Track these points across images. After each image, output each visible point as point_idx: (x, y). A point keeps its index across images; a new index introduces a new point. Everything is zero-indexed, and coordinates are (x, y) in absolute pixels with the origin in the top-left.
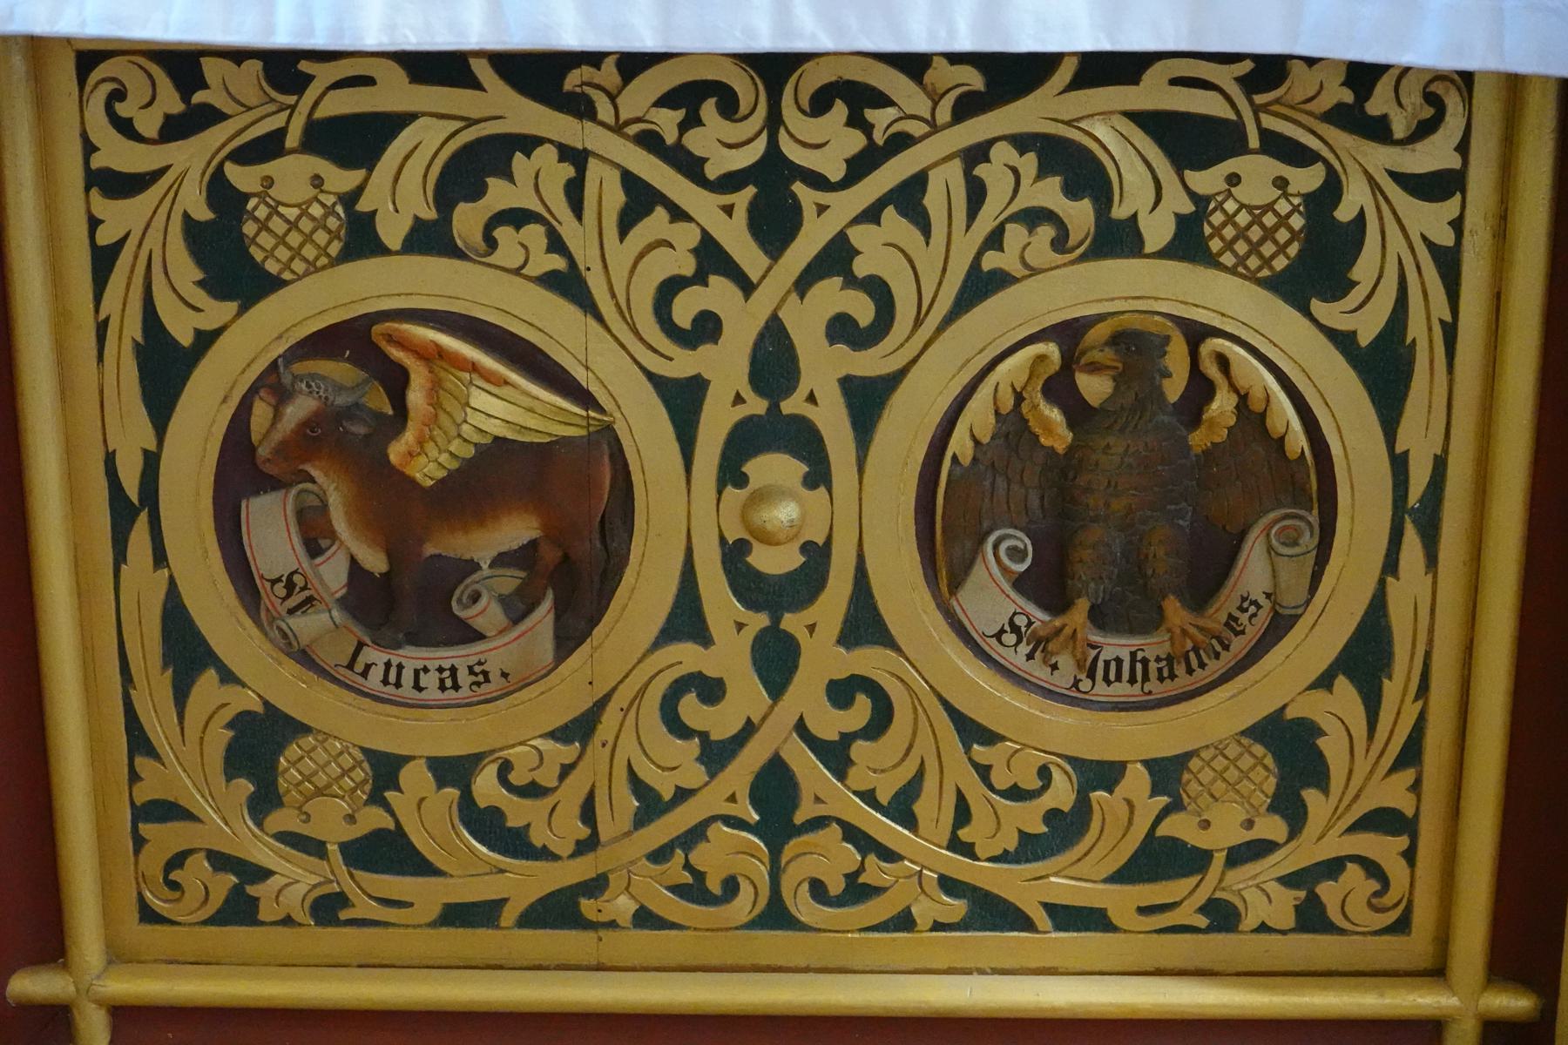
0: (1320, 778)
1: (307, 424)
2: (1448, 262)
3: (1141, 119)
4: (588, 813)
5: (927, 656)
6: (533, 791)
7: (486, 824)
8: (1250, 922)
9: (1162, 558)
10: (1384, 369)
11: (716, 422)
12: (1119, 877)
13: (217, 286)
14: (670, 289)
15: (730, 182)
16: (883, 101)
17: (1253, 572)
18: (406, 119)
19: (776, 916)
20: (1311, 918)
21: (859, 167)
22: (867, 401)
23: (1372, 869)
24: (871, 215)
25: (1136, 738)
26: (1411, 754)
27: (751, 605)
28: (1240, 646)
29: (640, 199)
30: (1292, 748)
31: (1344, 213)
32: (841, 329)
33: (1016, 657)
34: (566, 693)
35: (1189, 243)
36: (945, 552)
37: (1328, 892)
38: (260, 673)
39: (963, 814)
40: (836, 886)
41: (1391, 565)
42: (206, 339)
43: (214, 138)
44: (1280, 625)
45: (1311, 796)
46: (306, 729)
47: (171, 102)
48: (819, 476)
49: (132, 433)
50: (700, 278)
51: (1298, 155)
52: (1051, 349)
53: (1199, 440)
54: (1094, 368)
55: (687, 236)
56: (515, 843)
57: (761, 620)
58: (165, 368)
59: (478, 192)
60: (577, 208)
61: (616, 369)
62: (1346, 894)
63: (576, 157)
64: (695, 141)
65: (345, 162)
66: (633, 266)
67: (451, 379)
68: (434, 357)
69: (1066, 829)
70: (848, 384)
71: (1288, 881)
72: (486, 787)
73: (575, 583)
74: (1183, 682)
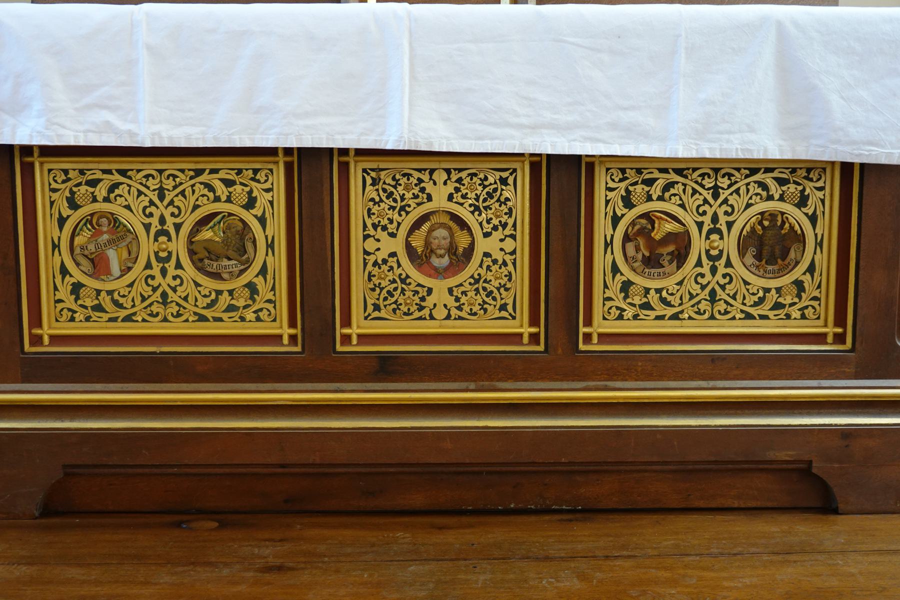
0: (804, 291)
1: (638, 230)
2: (823, 201)
3: (774, 178)
4: (681, 299)
5: (739, 269)
6: (672, 294)
7: (663, 301)
8: (793, 317)
9: (777, 252)
10: (813, 219)
11: (153, 231)
12: (770, 309)
13: (625, 206)
14: (699, 206)
15: (709, 189)
16: (178, 177)
17: (792, 255)
18: (657, 179)
19: (712, 317)
20: (803, 317)
21: (730, 186)
22: (730, 225)
23: (813, 307)
24: (731, 194)
25: (773, 284)
26: (819, 287)
27: (710, 260)
28: (790, 267)
29: (695, 192)
30: (799, 285)
31: (806, 193)
32: (726, 213)
33: (753, 270)
34: (678, 277)
35: (782, 199)
36: (742, 253)
37: (806, 311)
38: (77, 275)
39: (744, 298)
40: (723, 312)
41: (815, 253)
42: (623, 215)
43: (627, 182)
44: (797, 263)
45: (803, 294)
46: (85, 286)
47: (621, 176)
48: (722, 238)
49: (610, 231)
50: (704, 205)
51: (799, 184)
52: (759, 216)
53: (783, 232)
54: (766, 220)
55: (702, 198)
56: (669, 304)
57: (711, 263)
58: (616, 220)
59: (669, 191)
60: (684, 193)
61: (689, 220)
62: (809, 312)
63: (685, 185)
64: (704, 182)
65: (647, 186)
66: (693, 203)
67: (662, 222)
68: (657, 218)
69: (762, 300)
70: (727, 222)
71: (799, 310)
72: (664, 294)
73: (680, 257)
74: (781, 274)
